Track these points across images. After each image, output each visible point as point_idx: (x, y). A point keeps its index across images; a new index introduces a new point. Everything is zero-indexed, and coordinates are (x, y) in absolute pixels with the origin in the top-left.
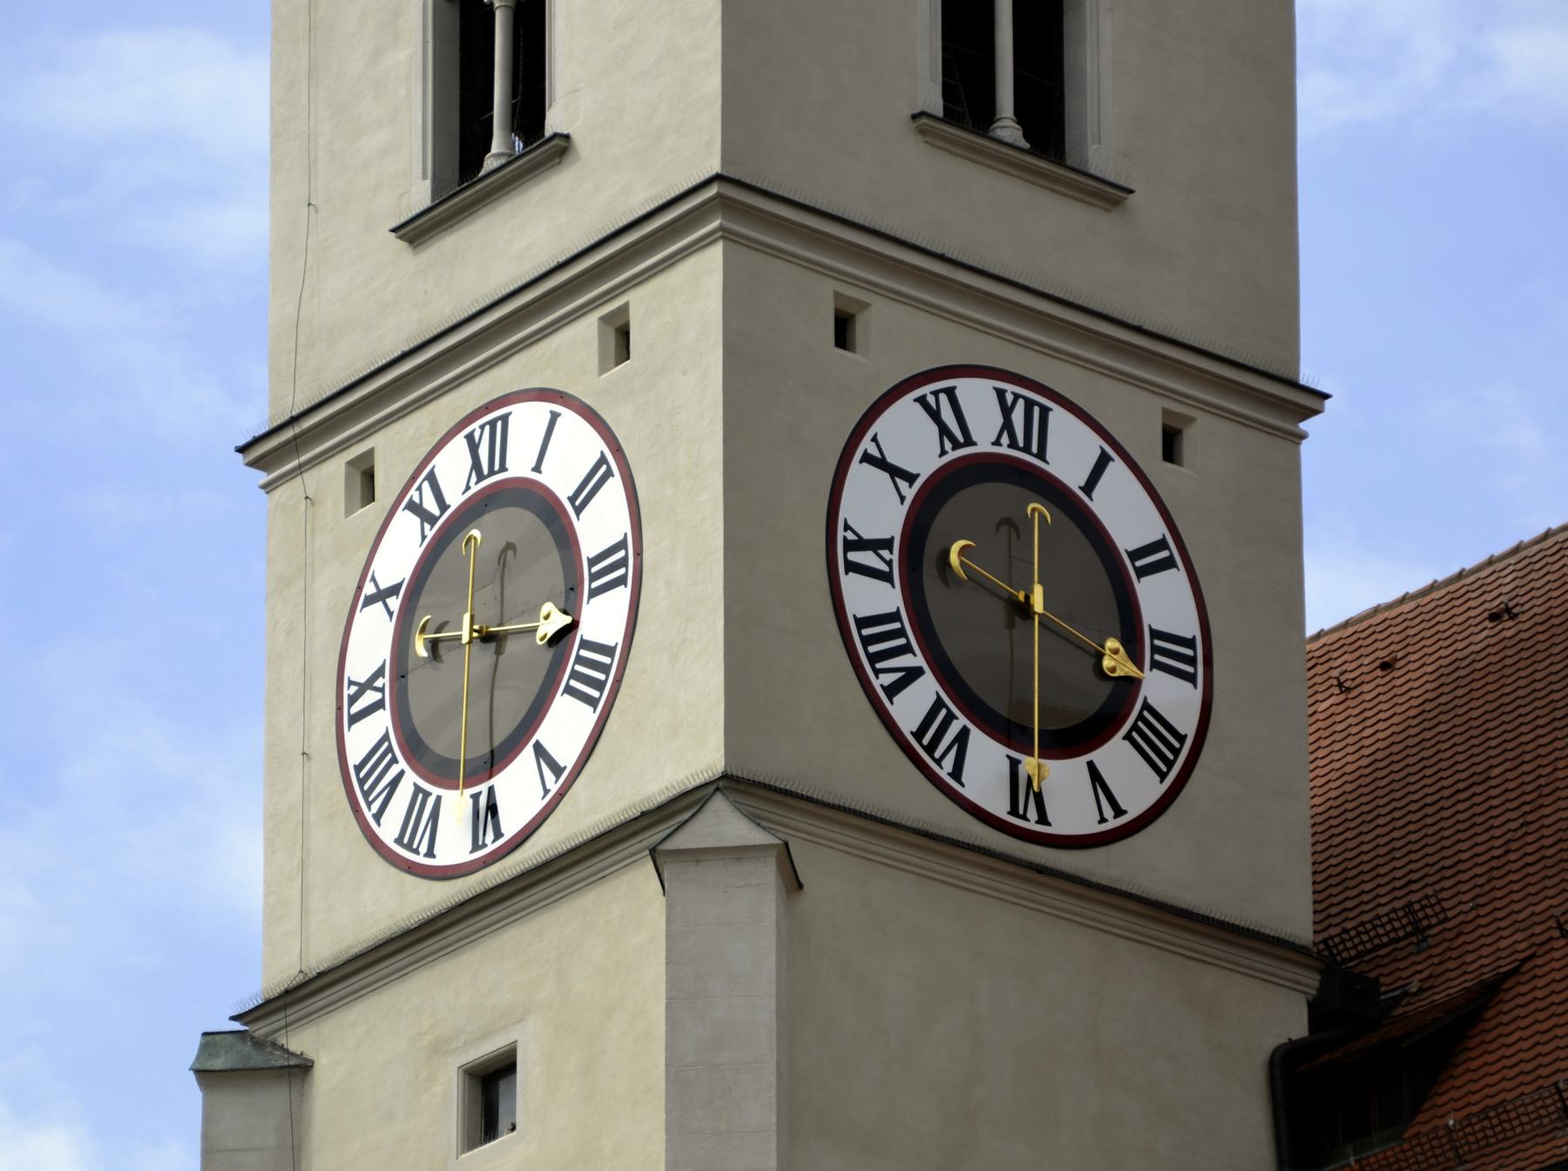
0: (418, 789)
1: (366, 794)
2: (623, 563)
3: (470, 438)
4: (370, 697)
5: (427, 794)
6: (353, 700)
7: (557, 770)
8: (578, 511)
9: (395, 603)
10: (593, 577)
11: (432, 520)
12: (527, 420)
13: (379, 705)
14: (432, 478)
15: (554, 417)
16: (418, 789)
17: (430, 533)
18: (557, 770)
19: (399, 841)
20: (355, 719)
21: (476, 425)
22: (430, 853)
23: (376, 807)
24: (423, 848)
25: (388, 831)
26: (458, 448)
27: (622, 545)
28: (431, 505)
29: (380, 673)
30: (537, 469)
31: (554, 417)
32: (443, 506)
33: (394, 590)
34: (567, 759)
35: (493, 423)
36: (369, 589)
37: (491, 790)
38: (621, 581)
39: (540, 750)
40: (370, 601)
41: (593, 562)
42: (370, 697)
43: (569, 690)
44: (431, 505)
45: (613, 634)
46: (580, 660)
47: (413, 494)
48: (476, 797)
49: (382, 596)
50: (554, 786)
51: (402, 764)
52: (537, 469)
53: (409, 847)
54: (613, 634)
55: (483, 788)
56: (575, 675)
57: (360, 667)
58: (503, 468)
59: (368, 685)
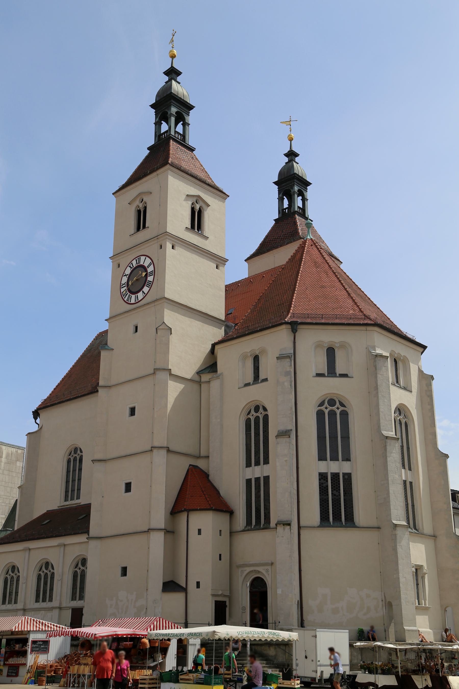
0: (129, 295)
1: (123, 295)
2: (153, 273)
3: (136, 260)
4: (124, 285)
5: (130, 295)
6: (122, 286)
7: (145, 294)
8: (148, 268)
9: (127, 276)
10: (149, 274)
11: (132, 268)
12: (143, 258)
13: (125, 286)
14: (132, 263)
15: (146, 258)
16: (129, 295)
17: (132, 269)
18: (145, 294)
19: (127, 300)
20: (122, 288)
21: (137, 258)
22: (130, 302)
23: (124, 297)
24: (129, 301)
25: (126, 299)
26: (135, 260)
27: (153, 271)
28: (132, 266)
29: (125, 283)
30: (143, 263)
31: (146, 258)
32: (133, 267)
33: (128, 275)
34: (146, 293)
35: (139, 258)
36: (124, 274)
37: (137, 295)
38: (152, 275)
39: (143, 292)
40: (124, 276)
41: (149, 273)
42: (124, 285)
43: (146, 286)
44: (132, 266)
45: (152, 280)
46: (148, 283)
47: (130, 265)
48: (135, 296)
49: (126, 275)
50: (144, 295)
51: (128, 292)
52: (143, 263)
53: (128, 301)
54: (152, 280)
55: (136, 295)
56: (147, 284)
57: (123, 282)
58: (140, 263)
59: (124, 284)
